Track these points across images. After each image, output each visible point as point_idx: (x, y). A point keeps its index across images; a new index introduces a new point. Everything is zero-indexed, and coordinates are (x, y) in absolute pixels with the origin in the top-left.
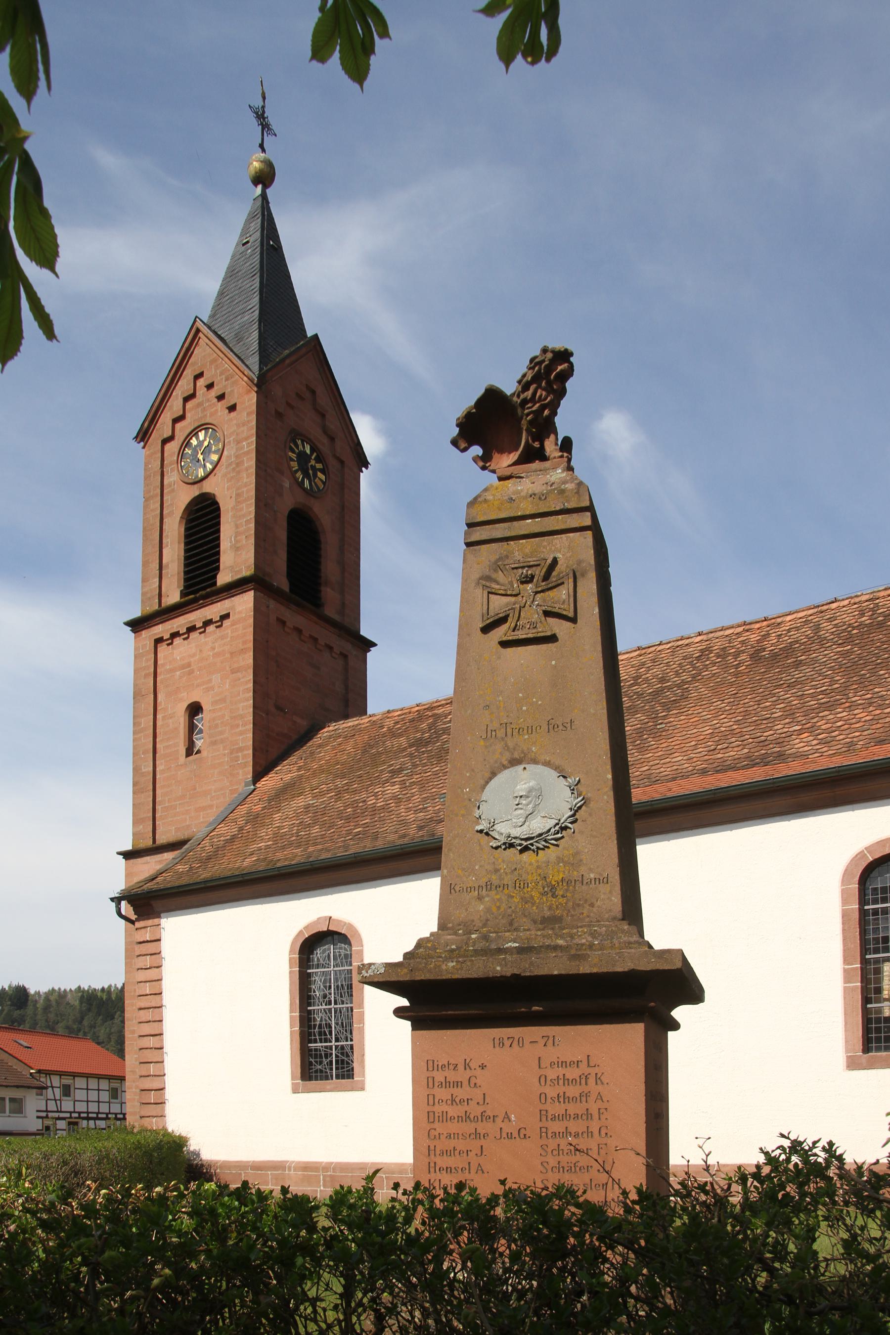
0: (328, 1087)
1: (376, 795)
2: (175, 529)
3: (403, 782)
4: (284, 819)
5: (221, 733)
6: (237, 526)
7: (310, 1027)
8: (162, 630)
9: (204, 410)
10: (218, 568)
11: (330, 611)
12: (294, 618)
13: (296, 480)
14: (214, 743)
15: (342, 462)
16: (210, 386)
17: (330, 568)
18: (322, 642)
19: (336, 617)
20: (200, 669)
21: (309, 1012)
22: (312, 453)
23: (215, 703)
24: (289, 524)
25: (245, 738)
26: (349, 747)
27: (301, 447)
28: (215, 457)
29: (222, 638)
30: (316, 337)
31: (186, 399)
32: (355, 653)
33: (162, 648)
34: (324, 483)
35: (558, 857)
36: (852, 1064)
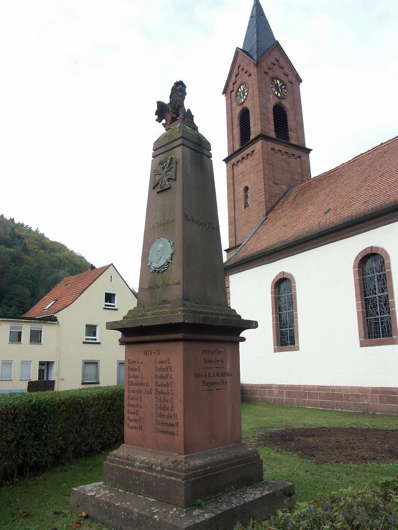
0: (286, 349)
2: (236, 122)
8: (234, 161)
12: (277, 147)
13: (275, 94)
16: (243, 69)
17: (291, 124)
19: (296, 143)
23: (253, 185)
28: (246, 94)
29: (253, 160)
32: (304, 155)
36: (363, 345)
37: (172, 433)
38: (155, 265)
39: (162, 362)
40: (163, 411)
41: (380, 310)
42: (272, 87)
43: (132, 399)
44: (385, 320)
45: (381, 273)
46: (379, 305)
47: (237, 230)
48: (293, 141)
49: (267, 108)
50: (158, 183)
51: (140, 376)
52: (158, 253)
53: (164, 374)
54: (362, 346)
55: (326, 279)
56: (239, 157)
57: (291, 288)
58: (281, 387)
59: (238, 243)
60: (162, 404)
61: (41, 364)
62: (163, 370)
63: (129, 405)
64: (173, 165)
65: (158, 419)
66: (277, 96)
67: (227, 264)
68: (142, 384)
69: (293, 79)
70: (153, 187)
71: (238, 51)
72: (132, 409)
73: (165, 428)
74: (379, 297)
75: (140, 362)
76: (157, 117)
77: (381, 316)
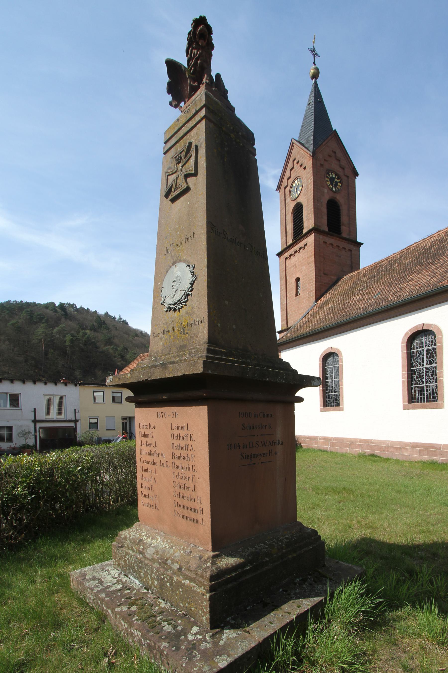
1: (353, 300)
2: (290, 218)
3: (363, 293)
4: (321, 315)
5: (306, 286)
6: (308, 211)
7: (326, 388)
8: (287, 255)
9: (297, 172)
10: (303, 229)
11: (345, 235)
12: (330, 240)
13: (329, 188)
14: (304, 290)
15: (348, 177)
16: (298, 163)
17: (344, 219)
18: (335, 245)
20: (299, 266)
21: (412, 371)
22: (335, 176)
23: (303, 276)
24: (327, 205)
25: (313, 287)
26: (348, 284)
27: (331, 176)
28: (300, 188)
29: (305, 253)
30: (335, 130)
31: (291, 170)
33: (287, 260)
34: (341, 187)
35: (186, 312)
36: (405, 408)
37: (195, 521)
38: (170, 301)
39: (179, 428)
40: (182, 491)
41: (426, 379)
42: (327, 181)
43: (146, 470)
44: (431, 388)
45: (431, 347)
46: (426, 375)
47: (288, 315)
48: (345, 235)
49: (321, 203)
50: (171, 187)
51: (154, 444)
52: (174, 284)
53: (183, 443)
54: (404, 409)
55: (372, 355)
56: (292, 251)
57: (338, 361)
58: (325, 439)
59: (289, 326)
60: (181, 481)
61: (124, 418)
62: (181, 438)
63: (142, 478)
64: (193, 153)
65: (177, 499)
66: (331, 190)
67: (281, 341)
68: (155, 454)
69: (348, 171)
70: (164, 194)
71: (293, 143)
72: (146, 484)
73: (186, 513)
74: (426, 368)
75: (152, 426)
76: (169, 98)
77: (427, 385)
